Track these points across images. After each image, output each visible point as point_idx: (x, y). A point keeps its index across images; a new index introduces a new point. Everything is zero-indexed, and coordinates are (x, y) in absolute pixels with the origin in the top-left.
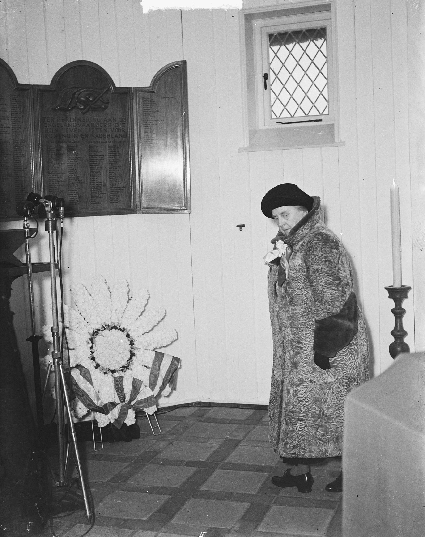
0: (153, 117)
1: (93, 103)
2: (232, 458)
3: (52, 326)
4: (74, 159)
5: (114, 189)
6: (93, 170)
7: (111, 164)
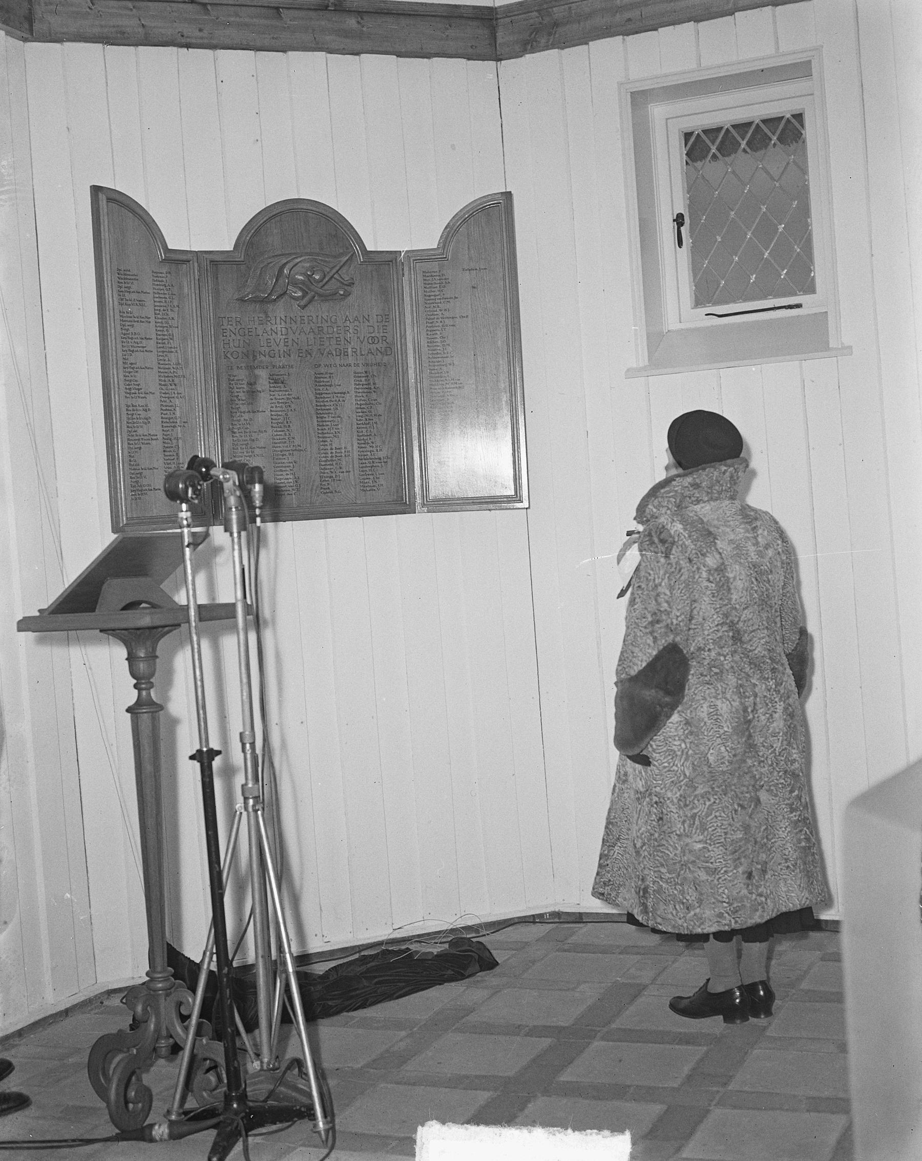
0: (445, 310)
1: (321, 284)
2: (627, 1019)
3: (241, 730)
4: (283, 401)
5: (367, 461)
6: (324, 423)
7: (360, 410)
